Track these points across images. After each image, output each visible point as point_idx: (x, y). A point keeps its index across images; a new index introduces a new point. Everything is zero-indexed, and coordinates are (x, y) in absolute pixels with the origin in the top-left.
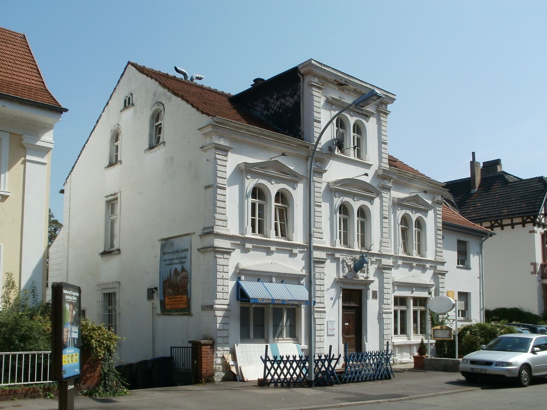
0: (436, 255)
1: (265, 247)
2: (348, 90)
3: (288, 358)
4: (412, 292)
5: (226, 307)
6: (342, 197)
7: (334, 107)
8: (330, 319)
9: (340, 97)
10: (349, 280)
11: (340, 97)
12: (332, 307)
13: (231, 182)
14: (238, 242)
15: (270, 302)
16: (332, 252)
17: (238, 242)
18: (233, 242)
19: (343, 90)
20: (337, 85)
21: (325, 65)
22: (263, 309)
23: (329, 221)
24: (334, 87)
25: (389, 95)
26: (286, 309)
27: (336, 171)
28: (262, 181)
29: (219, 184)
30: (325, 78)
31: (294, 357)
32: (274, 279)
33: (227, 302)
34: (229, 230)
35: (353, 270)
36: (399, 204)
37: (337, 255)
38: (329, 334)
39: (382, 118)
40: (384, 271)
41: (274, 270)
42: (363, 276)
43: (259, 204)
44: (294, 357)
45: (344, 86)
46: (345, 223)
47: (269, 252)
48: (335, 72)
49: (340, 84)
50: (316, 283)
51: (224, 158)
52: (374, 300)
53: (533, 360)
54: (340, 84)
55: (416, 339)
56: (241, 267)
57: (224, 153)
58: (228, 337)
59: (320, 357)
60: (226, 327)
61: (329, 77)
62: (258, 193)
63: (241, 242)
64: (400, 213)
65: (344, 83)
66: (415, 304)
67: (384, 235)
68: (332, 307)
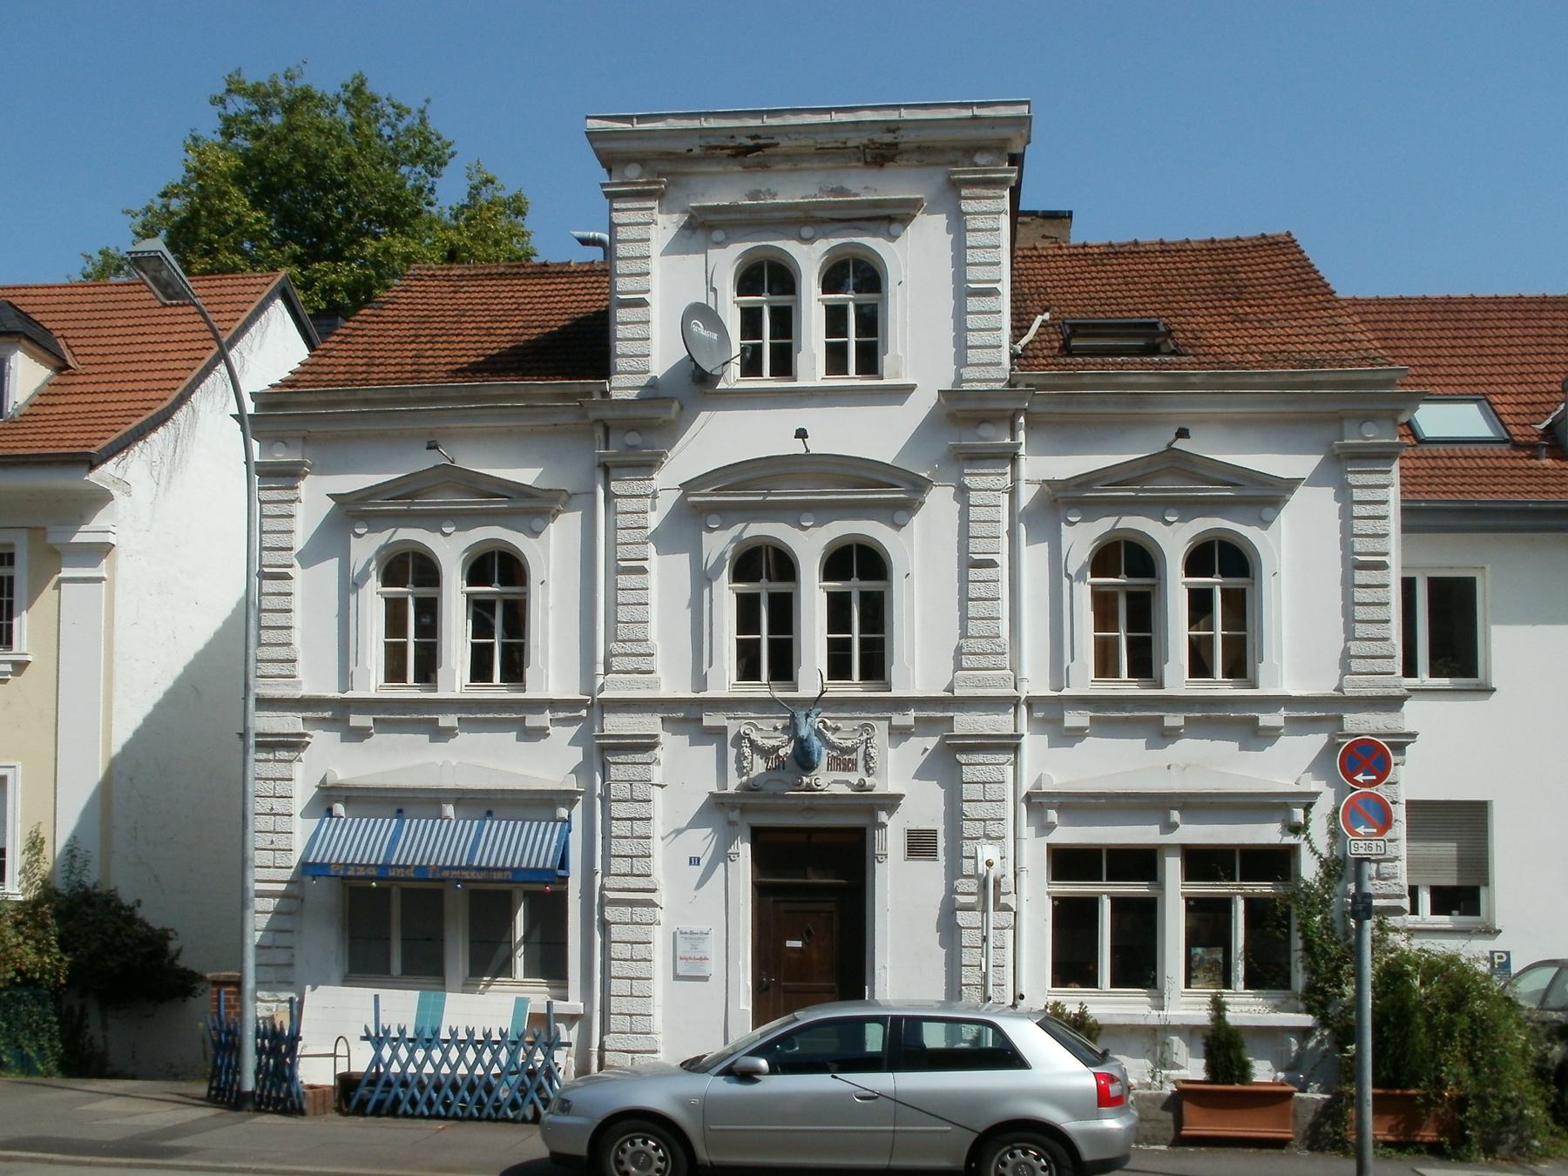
0: (1346, 669)
1: (1149, 721)
2: (788, 157)
3: (487, 1035)
4: (1170, 827)
5: (282, 887)
6: (740, 526)
7: (718, 235)
8: (686, 927)
9: (755, 195)
10: (768, 796)
11: (755, 195)
12: (699, 887)
13: (310, 557)
14: (327, 714)
15: (373, 872)
16: (688, 715)
17: (327, 714)
18: (309, 714)
19: (764, 166)
20: (734, 156)
21: (772, 113)
22: (440, 892)
23: (688, 613)
24: (808, 165)
25: (977, 112)
26: (527, 894)
27: (715, 441)
28: (405, 534)
29: (1360, 554)
30: (670, 154)
31: (402, 1032)
32: (339, 809)
33: (287, 875)
34: (298, 685)
35: (791, 765)
36: (1064, 499)
37: (710, 720)
38: (680, 972)
39: (966, 206)
40: (962, 758)
41: (449, 782)
42: (847, 783)
43: (1223, 591)
44: (402, 1032)
45: (767, 151)
46: (1143, 612)
47: (440, 734)
48: (695, 124)
49: (741, 152)
50: (615, 814)
51: (285, 495)
52: (921, 866)
53: (707, 1107)
54: (741, 152)
55: (1186, 1004)
56: (330, 782)
57: (283, 482)
58: (290, 965)
59: (454, 1033)
60: (283, 939)
61: (680, 146)
62: (748, 563)
63: (337, 713)
64: (366, 547)
65: (750, 143)
66: (1190, 874)
67: (973, 627)
68: (699, 887)
